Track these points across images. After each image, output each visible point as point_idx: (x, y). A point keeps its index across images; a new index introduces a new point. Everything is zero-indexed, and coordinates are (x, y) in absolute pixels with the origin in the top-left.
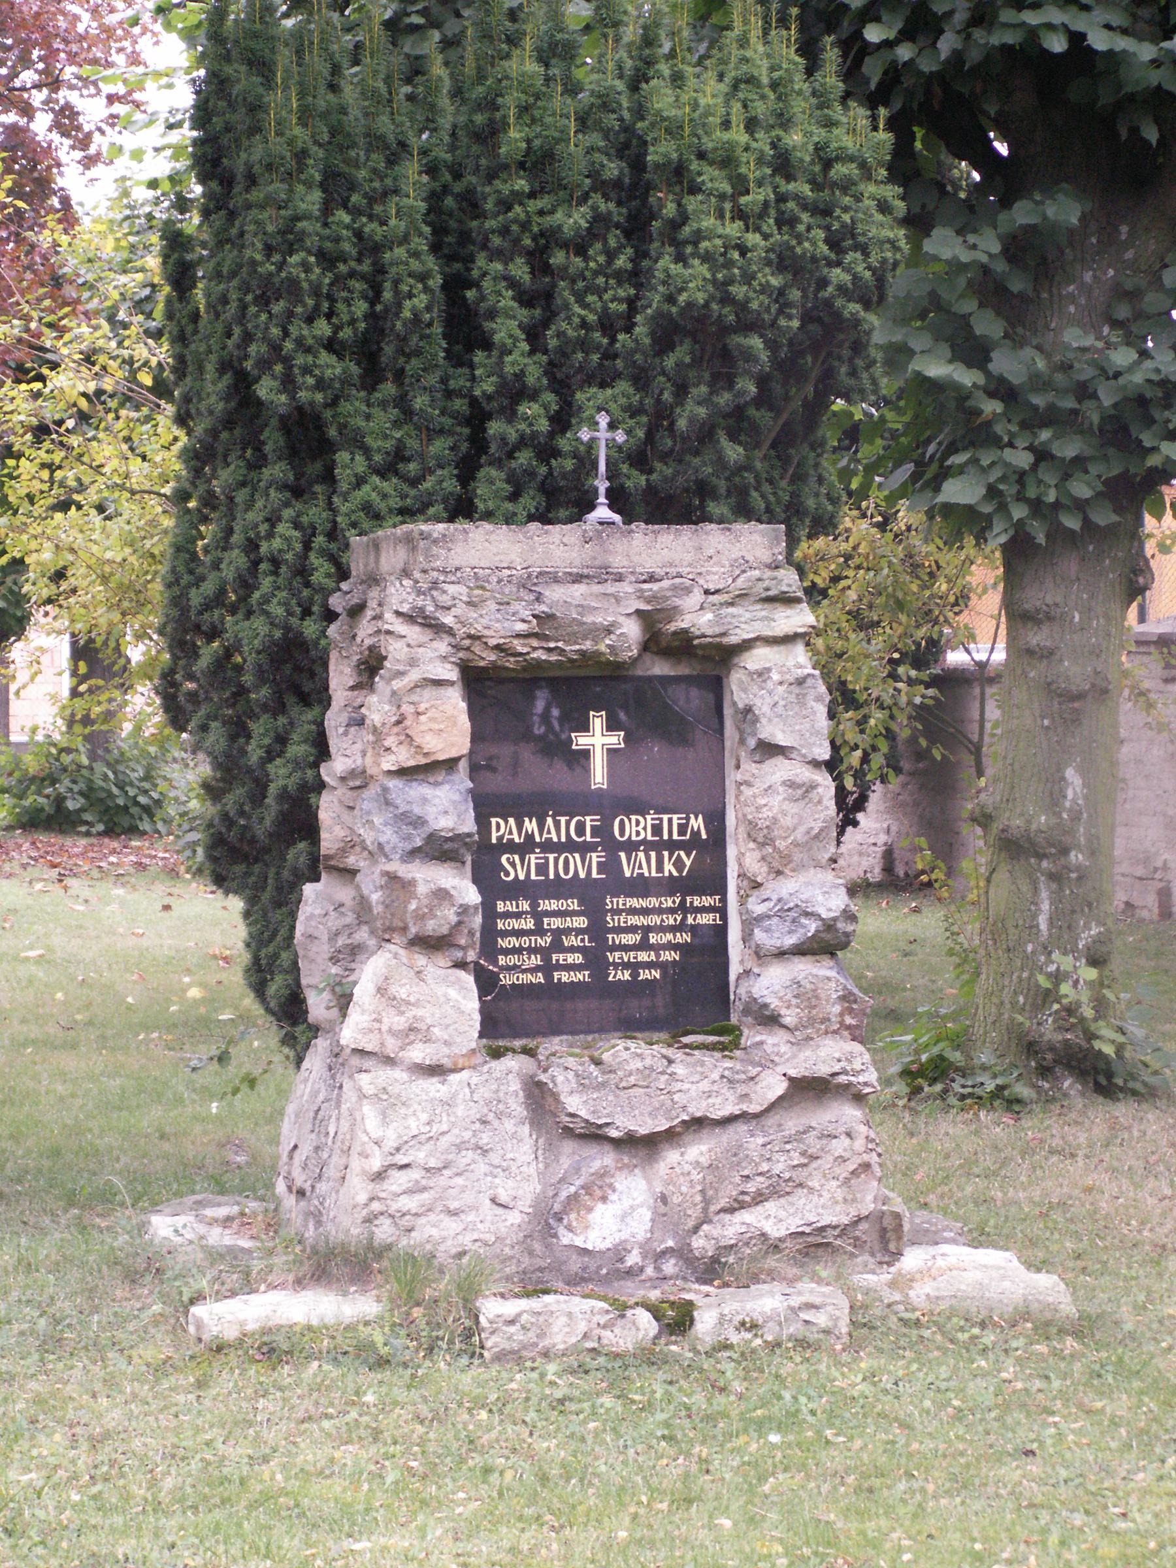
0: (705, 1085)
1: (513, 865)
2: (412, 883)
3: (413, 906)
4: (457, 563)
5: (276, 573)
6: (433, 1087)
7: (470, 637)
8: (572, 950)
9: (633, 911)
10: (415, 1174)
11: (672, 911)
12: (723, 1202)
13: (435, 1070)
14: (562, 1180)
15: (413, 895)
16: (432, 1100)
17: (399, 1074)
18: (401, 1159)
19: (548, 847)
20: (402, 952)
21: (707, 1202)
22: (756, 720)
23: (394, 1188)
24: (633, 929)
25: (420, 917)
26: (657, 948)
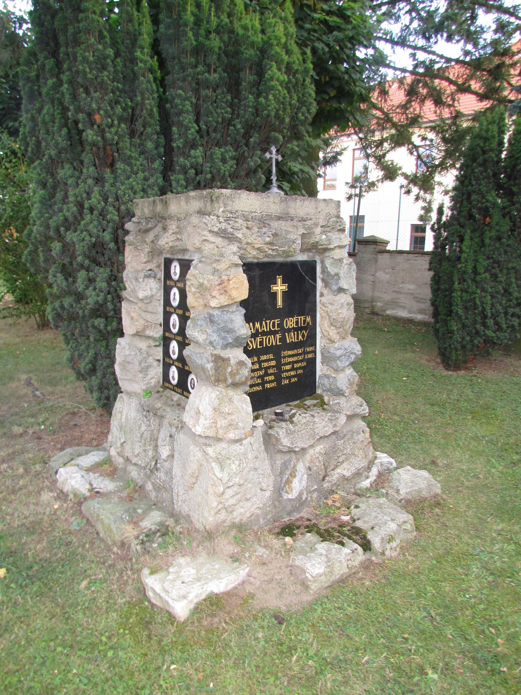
0: (324, 423)
1: (251, 342)
2: (228, 359)
3: (229, 369)
4: (236, 208)
5: (92, 213)
6: (237, 447)
7: (247, 243)
8: (271, 374)
9: (290, 356)
10: (235, 489)
11: (300, 354)
12: (332, 467)
13: (238, 441)
14: (281, 473)
15: (229, 365)
16: (238, 454)
17: (224, 445)
18: (230, 484)
19: (264, 333)
20: (223, 390)
21: (326, 468)
22: (339, 278)
23: (227, 496)
24: (289, 363)
25: (232, 374)
26: (297, 369)
